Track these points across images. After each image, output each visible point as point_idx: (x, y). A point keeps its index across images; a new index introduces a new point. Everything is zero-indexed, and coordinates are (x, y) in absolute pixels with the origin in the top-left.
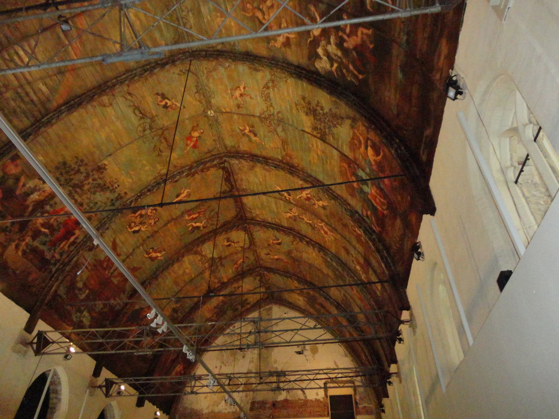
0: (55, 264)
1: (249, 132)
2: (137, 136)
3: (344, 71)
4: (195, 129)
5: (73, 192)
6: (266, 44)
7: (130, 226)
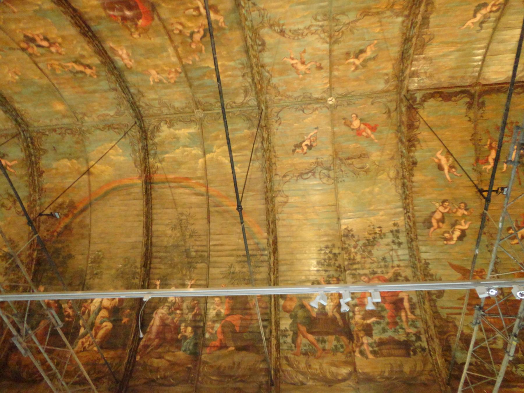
0: (419, 339)
1: (359, 60)
2: (333, 186)
4: (348, 123)
5: (354, 272)
7: (446, 239)
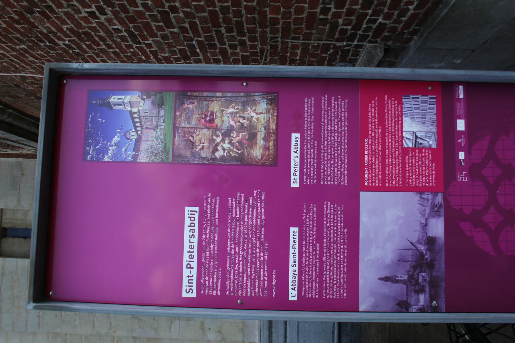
6: (191, 150)
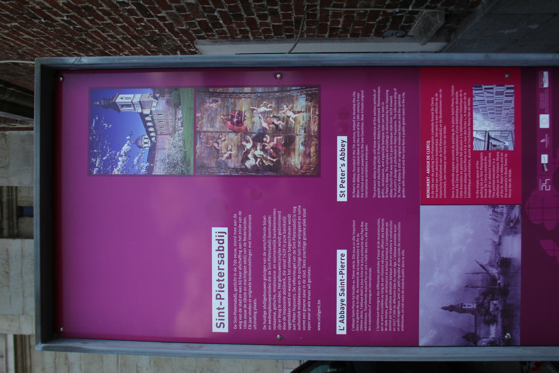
3: (264, 161)
